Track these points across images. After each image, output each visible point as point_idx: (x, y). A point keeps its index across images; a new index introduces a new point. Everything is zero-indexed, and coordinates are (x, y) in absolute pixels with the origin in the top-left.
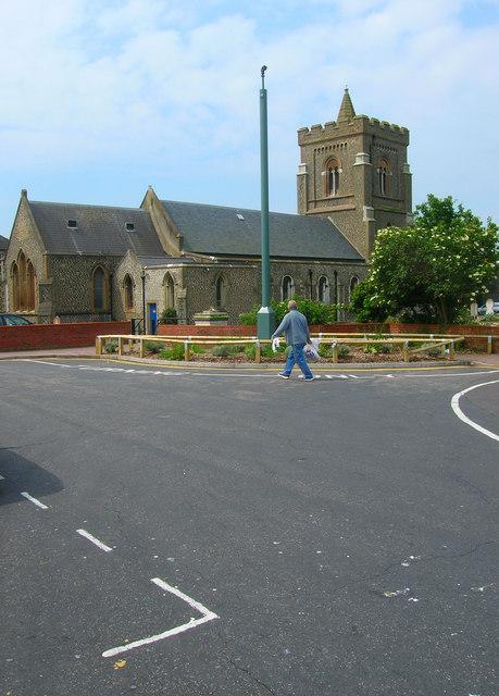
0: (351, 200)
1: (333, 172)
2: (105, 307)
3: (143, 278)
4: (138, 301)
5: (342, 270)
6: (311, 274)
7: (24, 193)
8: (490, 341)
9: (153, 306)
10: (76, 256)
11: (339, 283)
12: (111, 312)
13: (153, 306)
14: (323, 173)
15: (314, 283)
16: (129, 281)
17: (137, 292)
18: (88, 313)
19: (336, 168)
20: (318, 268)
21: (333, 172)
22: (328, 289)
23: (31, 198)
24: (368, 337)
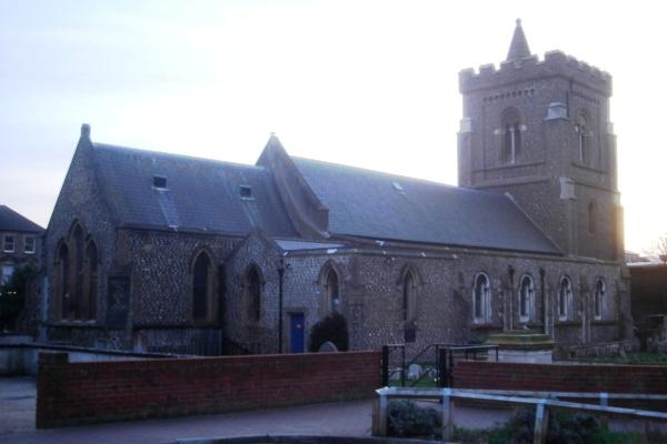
0: (540, 168)
1: (512, 130)
2: (211, 315)
3: (281, 272)
4: (270, 309)
5: (549, 266)
6: (511, 271)
7: (86, 130)
8: (540, 413)
9: (298, 316)
10: (170, 232)
11: (547, 287)
12: (221, 322)
13: (298, 316)
14: (497, 132)
15: (515, 286)
16: (254, 275)
17: (269, 292)
18: (182, 327)
19: (517, 126)
20: (521, 265)
21: (512, 130)
22: (571, 296)
23: (97, 138)
24: (612, 402)
